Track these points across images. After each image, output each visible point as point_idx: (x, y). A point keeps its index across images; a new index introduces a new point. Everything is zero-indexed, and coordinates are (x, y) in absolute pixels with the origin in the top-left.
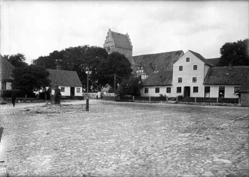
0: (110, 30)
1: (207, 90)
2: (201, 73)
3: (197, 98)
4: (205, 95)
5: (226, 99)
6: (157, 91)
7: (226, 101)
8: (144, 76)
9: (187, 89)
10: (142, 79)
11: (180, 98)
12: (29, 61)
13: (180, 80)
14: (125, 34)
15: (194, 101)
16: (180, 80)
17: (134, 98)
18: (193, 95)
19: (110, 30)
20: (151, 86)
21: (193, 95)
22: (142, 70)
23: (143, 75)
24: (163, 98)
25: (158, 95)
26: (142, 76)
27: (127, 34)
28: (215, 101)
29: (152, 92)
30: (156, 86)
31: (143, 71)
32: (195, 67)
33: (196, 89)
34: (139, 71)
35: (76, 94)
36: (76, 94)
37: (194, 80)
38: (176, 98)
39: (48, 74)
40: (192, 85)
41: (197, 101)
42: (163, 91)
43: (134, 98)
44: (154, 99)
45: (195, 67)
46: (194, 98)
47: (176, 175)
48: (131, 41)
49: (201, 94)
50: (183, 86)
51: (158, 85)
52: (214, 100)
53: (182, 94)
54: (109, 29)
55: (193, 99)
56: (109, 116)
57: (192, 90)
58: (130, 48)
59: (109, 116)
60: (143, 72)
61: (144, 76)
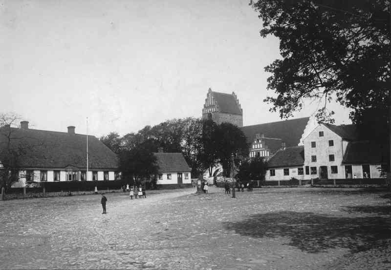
0: (210, 89)
1: (349, 170)
2: (340, 146)
3: (337, 180)
4: (347, 176)
5: (355, 179)
6: (286, 173)
7: (270, 183)
8: (263, 152)
9: (324, 169)
10: (261, 156)
11: (316, 181)
12: (76, 132)
13: (314, 159)
14: (230, 93)
15: (278, 185)
16: (314, 159)
17: (258, 183)
18: (331, 176)
19: (210, 89)
20: (278, 167)
21: (331, 176)
22: (260, 144)
23: (262, 151)
24: (294, 182)
25: (288, 178)
26: (261, 152)
27: (233, 93)
28: (337, 182)
29: (279, 175)
30: (284, 166)
31: (261, 145)
32: (331, 143)
33: (335, 169)
34: (256, 145)
35: (185, 181)
36: (185, 181)
37: (332, 158)
38: (311, 180)
39: (155, 159)
40: (329, 165)
41: (281, 185)
42: (294, 173)
43: (258, 183)
44: (284, 183)
45: (331, 143)
46: (332, 180)
47: (343, 131)
48: (239, 103)
49: (341, 174)
50: (318, 165)
51: (288, 166)
52: (357, 181)
53: (317, 176)
54: (208, 89)
55: (331, 182)
56: (130, 229)
57: (329, 170)
58: (239, 112)
59: (130, 229)
60: (261, 146)
61: (263, 152)
